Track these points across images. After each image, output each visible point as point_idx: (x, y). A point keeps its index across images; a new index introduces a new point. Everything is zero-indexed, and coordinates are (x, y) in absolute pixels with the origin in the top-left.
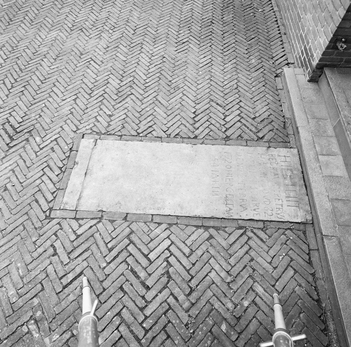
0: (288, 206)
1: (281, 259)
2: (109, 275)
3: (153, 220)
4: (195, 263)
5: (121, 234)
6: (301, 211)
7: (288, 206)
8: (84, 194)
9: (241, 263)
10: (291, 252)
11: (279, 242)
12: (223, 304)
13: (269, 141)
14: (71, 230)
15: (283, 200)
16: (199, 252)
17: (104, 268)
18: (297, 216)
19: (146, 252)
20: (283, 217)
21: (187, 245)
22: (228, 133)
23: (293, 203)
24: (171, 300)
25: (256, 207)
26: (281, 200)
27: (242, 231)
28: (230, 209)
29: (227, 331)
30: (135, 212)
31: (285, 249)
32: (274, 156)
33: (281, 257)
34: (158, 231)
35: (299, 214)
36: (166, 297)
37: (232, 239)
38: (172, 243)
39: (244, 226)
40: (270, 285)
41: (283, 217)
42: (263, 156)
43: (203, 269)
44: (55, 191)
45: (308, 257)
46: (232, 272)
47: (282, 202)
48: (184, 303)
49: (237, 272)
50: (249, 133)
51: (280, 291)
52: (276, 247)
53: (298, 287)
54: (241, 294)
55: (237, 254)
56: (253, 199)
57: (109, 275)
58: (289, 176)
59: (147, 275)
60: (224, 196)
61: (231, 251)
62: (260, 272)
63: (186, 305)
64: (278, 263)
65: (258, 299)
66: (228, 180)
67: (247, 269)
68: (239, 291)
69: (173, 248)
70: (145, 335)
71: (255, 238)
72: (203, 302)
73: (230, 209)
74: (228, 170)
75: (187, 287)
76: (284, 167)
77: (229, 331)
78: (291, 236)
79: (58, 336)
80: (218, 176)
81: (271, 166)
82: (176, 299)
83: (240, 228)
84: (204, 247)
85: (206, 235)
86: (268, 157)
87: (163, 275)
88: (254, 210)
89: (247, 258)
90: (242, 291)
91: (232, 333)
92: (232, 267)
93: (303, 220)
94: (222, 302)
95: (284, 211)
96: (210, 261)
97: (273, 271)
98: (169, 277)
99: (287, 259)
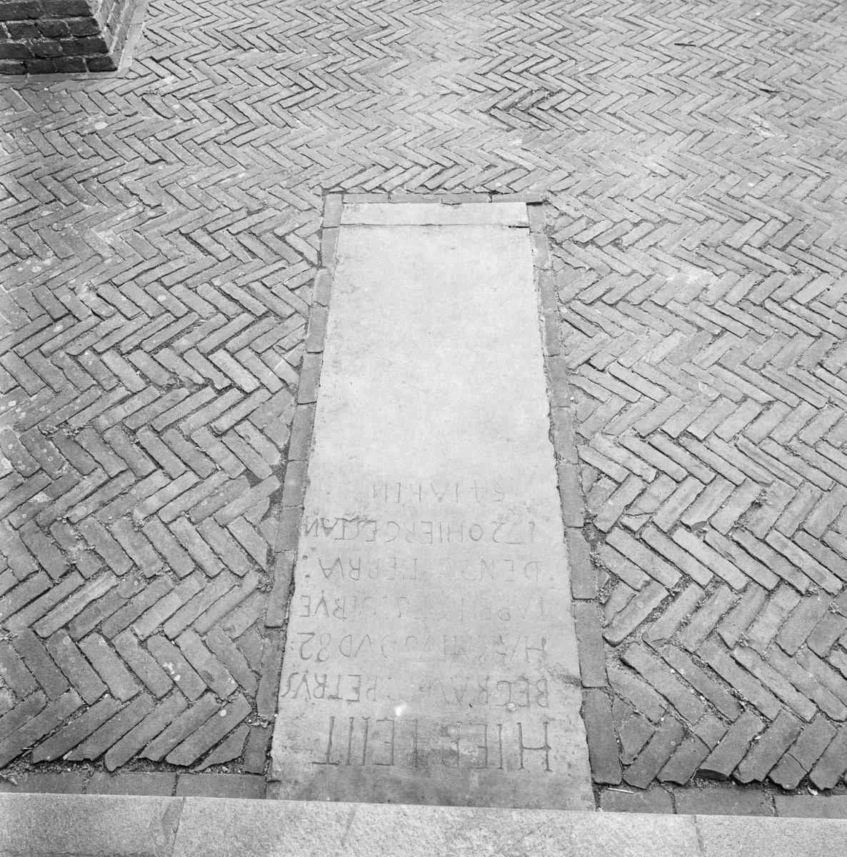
0: (333, 718)
1: (165, 665)
2: (196, 292)
3: (307, 368)
4: (193, 441)
5: (280, 301)
6: (313, 769)
7: (333, 718)
8: (378, 232)
9: (171, 547)
10: (181, 702)
11: (215, 669)
12: (86, 497)
13: (609, 688)
14: (297, 226)
15: (356, 704)
16: (216, 450)
17: (211, 284)
18: (295, 749)
19: (230, 345)
20: (291, 694)
21: (236, 424)
22: (616, 537)
23: (341, 742)
24: (121, 392)
25: (332, 606)
26: (354, 696)
27: (262, 559)
28: (328, 530)
29: (31, 505)
30: (330, 319)
31: (194, 683)
32: (542, 700)
33: (170, 666)
34: (281, 365)
35: (299, 757)
36: (127, 385)
37: (242, 531)
38: (247, 395)
39: (274, 576)
40: (101, 618)
41: (291, 694)
42: (534, 656)
43: (173, 457)
44: (385, 190)
45: (155, 757)
46: (155, 521)
47: (350, 701)
48: (108, 419)
49: (151, 535)
50: (634, 611)
51: (81, 645)
52: (202, 659)
53: (79, 702)
54: (98, 541)
55: (198, 540)
56: (359, 601)
57: (196, 292)
58: (454, 747)
59: (182, 350)
60: (372, 516)
61: (208, 525)
62: (141, 597)
63: (103, 422)
64: (158, 653)
65: (75, 579)
66: (426, 528)
67: (154, 563)
68: (107, 536)
69: (234, 395)
70: (70, 355)
71: (237, 595)
72: (102, 455)
73: (328, 530)
74: (466, 531)
75: (140, 423)
76: (493, 732)
77: (31, 509)
78: (229, 712)
79: (109, 243)
80: (440, 499)
81: (492, 683)
82: (122, 401)
83: (271, 560)
84: (229, 461)
85: (262, 469)
86: (534, 675)
87: (174, 374)
88: (323, 601)
89: (185, 567)
90: (104, 542)
91: (24, 516)
92: (166, 525)
93: (276, 767)
94: (91, 494)
95: (313, 700)
96: (191, 474)
97: (136, 635)
98: (169, 388)
99: (161, 689)
